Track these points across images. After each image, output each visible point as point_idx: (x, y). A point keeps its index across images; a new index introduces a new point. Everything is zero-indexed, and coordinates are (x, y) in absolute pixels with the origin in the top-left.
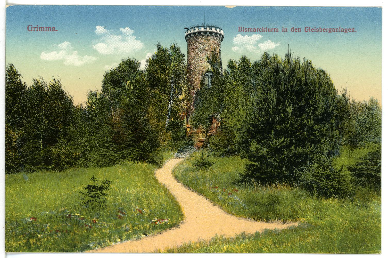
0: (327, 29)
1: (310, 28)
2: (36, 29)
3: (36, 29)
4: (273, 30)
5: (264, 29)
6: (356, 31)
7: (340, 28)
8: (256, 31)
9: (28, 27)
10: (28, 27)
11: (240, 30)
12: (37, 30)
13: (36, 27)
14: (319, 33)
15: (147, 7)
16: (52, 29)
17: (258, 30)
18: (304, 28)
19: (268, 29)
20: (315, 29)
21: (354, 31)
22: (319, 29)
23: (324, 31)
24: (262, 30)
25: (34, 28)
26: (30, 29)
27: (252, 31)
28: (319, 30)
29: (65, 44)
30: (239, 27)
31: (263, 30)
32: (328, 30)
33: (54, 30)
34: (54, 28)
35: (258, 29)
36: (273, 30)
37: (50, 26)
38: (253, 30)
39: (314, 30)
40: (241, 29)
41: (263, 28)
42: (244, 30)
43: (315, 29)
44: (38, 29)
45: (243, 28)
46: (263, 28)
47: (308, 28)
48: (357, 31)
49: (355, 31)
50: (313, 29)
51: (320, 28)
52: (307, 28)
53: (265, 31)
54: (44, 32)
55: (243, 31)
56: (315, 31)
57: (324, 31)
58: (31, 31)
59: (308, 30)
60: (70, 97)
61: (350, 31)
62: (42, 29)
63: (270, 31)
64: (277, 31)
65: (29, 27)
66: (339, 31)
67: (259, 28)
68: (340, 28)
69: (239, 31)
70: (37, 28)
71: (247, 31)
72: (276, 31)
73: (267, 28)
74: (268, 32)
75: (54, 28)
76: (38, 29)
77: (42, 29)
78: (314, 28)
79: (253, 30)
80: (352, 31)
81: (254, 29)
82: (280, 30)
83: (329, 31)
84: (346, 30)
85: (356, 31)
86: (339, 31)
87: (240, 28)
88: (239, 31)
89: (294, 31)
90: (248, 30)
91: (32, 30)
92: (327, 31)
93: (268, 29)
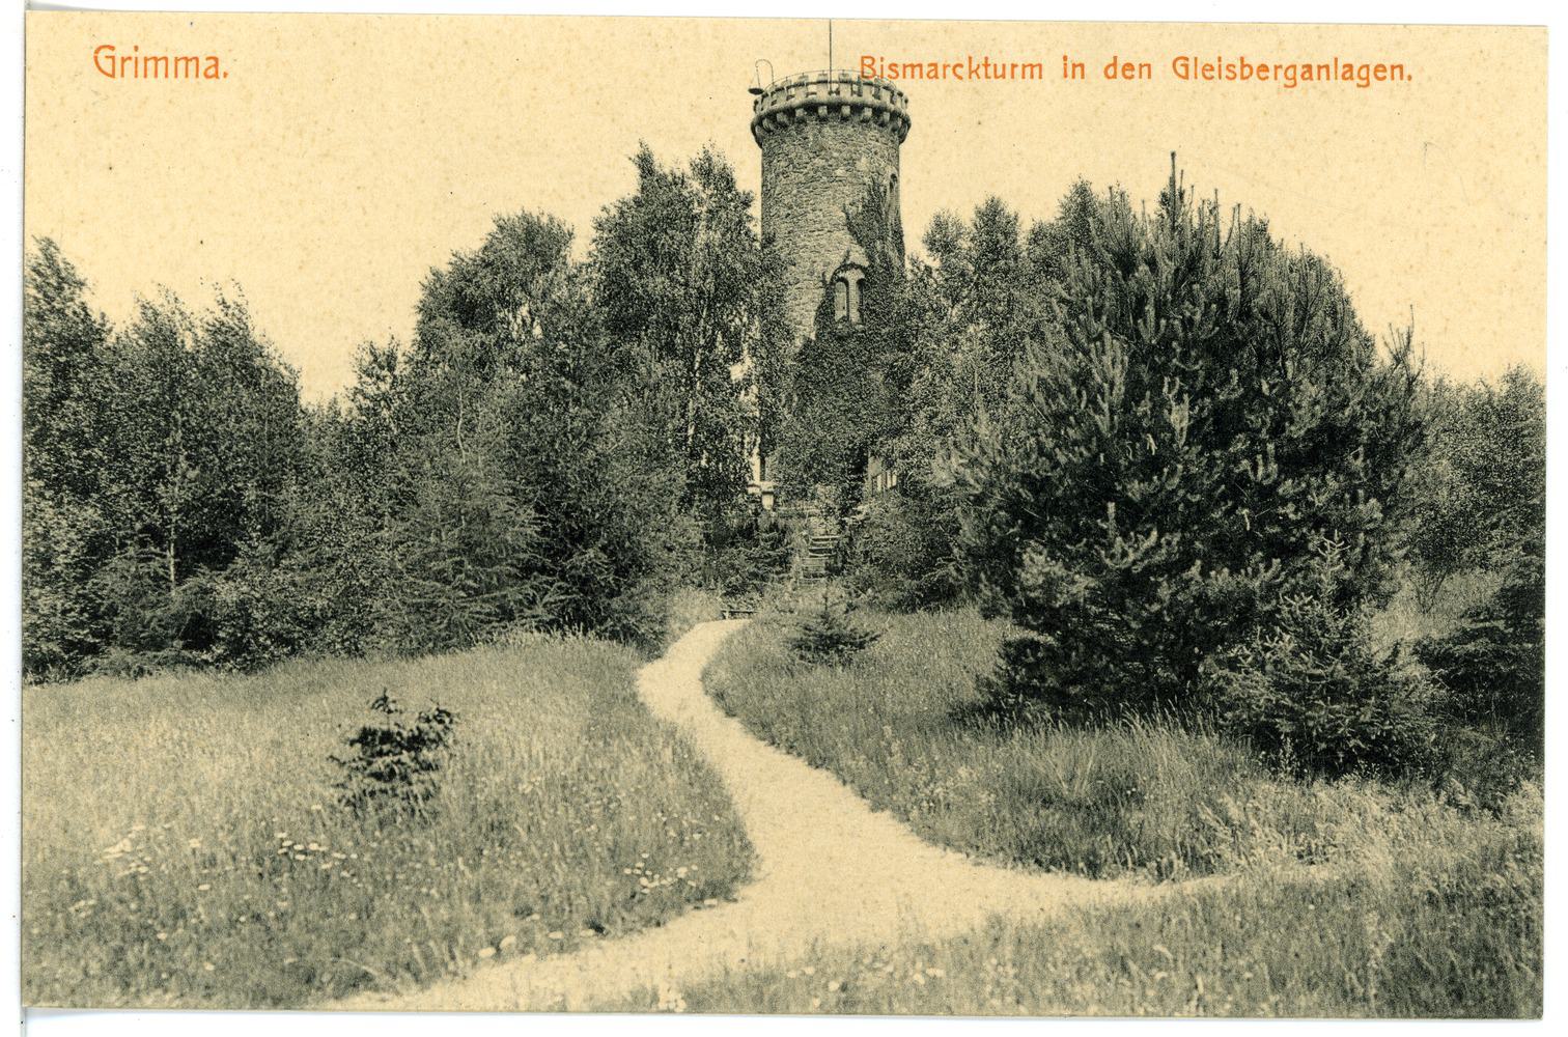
0: (1014, 66)
4: (1018, 71)
36: (1018, 71)
39: (1215, 73)
49: (1406, 74)
50: (1212, 69)
79: (926, 69)
82: (1094, 70)
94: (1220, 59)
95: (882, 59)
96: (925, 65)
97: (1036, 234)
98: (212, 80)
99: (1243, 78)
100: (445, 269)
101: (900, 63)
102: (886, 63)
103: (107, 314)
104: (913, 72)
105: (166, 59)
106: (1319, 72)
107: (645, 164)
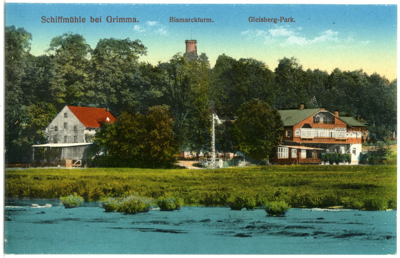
0: (189, 19)
1: (254, 18)
2: (115, 20)
3: (115, 20)
4: (206, 20)
5: (197, 19)
6: (138, 22)
7: (80, 17)
8: (203, 21)
9: (249, 19)
10: (249, 19)
11: (172, 21)
12: (117, 22)
13: (116, 18)
14: (74, 24)
15: (334, 6)
16: (132, 20)
17: (190, 20)
18: (248, 20)
19: (201, 19)
20: (259, 19)
21: (211, 22)
22: (264, 18)
23: (269, 21)
24: (194, 20)
25: (114, 19)
26: (251, 20)
27: (131, 22)
28: (264, 20)
29: (329, 32)
30: (281, 17)
31: (196, 21)
32: (273, 20)
33: (134, 21)
34: (134, 19)
35: (205, 19)
36: (206, 20)
37: (184, 18)
38: (132, 20)
39: (259, 20)
40: (172, 19)
41: (195, 18)
42: (176, 20)
43: (259, 19)
44: (118, 20)
45: (174, 18)
46: (195, 18)
47: (252, 18)
48: (139, 21)
49: (212, 21)
50: (258, 19)
51: (264, 18)
52: (251, 19)
53: (197, 21)
54: (61, 23)
55: (174, 21)
56: (260, 21)
57: (257, 21)
58: (252, 23)
59: (252, 19)
60: (50, 177)
61: (270, 21)
62: (122, 20)
63: (202, 21)
64: (210, 21)
65: (108, 18)
66: (79, 21)
67: (191, 19)
68: (80, 17)
69: (170, 22)
70: (117, 19)
71: (178, 21)
72: (122, 22)
73: (200, 18)
74: (70, 23)
75: (134, 19)
76: (118, 20)
77: (122, 20)
78: (99, 18)
79: (185, 20)
80: (51, 22)
81: (186, 19)
82: (104, 20)
83: (274, 21)
84: (275, 20)
85: (213, 22)
86: (79, 21)
87: (172, 18)
88: (170, 22)
89: (81, 21)
90: (179, 20)
91: (111, 21)
92: (272, 21)
93: (201, 19)
94: (259, 17)
95: (175, 18)
96: (132, 18)
97: (375, 79)
98: (202, 22)
99: (265, 21)
100: (313, 70)
101: (179, 18)
102: (176, 19)
103: (218, 220)
104: (66, 20)
105: (68, 19)
106: (73, 20)
107: (159, 62)
